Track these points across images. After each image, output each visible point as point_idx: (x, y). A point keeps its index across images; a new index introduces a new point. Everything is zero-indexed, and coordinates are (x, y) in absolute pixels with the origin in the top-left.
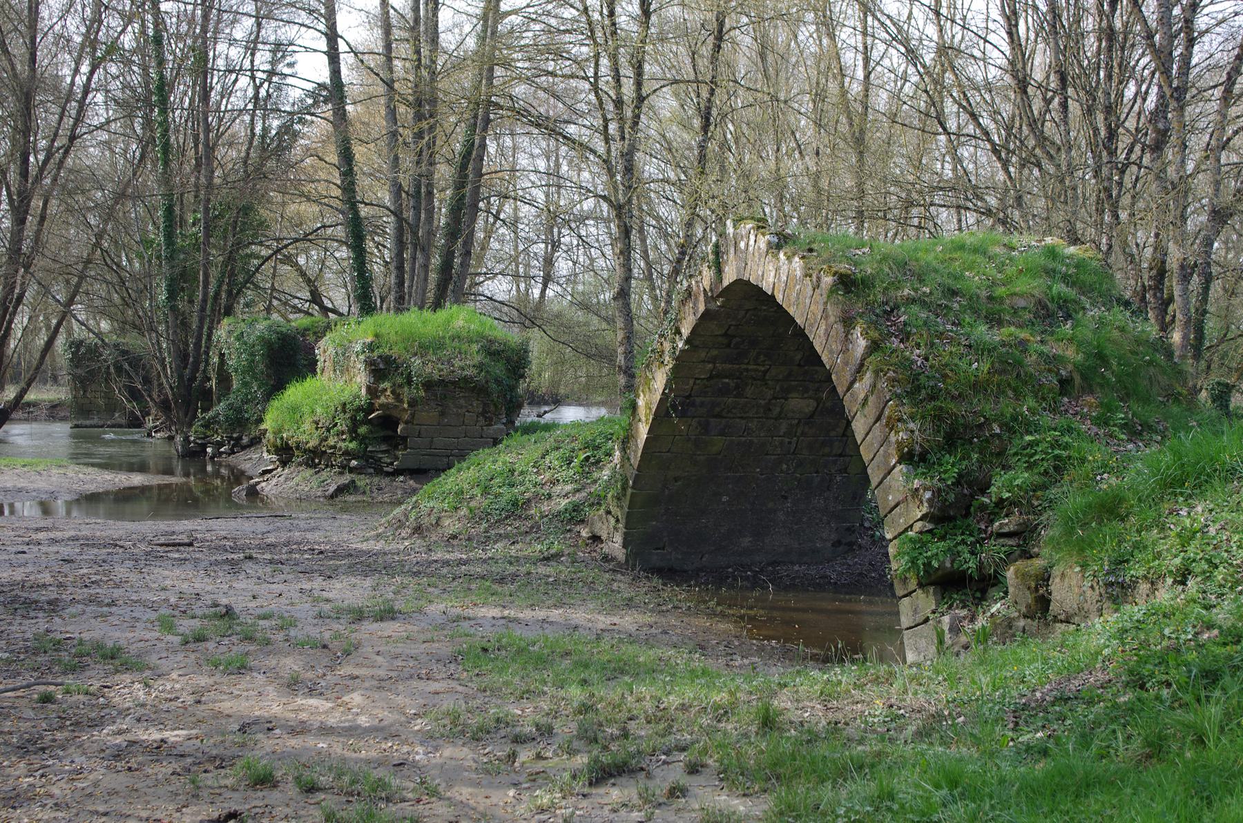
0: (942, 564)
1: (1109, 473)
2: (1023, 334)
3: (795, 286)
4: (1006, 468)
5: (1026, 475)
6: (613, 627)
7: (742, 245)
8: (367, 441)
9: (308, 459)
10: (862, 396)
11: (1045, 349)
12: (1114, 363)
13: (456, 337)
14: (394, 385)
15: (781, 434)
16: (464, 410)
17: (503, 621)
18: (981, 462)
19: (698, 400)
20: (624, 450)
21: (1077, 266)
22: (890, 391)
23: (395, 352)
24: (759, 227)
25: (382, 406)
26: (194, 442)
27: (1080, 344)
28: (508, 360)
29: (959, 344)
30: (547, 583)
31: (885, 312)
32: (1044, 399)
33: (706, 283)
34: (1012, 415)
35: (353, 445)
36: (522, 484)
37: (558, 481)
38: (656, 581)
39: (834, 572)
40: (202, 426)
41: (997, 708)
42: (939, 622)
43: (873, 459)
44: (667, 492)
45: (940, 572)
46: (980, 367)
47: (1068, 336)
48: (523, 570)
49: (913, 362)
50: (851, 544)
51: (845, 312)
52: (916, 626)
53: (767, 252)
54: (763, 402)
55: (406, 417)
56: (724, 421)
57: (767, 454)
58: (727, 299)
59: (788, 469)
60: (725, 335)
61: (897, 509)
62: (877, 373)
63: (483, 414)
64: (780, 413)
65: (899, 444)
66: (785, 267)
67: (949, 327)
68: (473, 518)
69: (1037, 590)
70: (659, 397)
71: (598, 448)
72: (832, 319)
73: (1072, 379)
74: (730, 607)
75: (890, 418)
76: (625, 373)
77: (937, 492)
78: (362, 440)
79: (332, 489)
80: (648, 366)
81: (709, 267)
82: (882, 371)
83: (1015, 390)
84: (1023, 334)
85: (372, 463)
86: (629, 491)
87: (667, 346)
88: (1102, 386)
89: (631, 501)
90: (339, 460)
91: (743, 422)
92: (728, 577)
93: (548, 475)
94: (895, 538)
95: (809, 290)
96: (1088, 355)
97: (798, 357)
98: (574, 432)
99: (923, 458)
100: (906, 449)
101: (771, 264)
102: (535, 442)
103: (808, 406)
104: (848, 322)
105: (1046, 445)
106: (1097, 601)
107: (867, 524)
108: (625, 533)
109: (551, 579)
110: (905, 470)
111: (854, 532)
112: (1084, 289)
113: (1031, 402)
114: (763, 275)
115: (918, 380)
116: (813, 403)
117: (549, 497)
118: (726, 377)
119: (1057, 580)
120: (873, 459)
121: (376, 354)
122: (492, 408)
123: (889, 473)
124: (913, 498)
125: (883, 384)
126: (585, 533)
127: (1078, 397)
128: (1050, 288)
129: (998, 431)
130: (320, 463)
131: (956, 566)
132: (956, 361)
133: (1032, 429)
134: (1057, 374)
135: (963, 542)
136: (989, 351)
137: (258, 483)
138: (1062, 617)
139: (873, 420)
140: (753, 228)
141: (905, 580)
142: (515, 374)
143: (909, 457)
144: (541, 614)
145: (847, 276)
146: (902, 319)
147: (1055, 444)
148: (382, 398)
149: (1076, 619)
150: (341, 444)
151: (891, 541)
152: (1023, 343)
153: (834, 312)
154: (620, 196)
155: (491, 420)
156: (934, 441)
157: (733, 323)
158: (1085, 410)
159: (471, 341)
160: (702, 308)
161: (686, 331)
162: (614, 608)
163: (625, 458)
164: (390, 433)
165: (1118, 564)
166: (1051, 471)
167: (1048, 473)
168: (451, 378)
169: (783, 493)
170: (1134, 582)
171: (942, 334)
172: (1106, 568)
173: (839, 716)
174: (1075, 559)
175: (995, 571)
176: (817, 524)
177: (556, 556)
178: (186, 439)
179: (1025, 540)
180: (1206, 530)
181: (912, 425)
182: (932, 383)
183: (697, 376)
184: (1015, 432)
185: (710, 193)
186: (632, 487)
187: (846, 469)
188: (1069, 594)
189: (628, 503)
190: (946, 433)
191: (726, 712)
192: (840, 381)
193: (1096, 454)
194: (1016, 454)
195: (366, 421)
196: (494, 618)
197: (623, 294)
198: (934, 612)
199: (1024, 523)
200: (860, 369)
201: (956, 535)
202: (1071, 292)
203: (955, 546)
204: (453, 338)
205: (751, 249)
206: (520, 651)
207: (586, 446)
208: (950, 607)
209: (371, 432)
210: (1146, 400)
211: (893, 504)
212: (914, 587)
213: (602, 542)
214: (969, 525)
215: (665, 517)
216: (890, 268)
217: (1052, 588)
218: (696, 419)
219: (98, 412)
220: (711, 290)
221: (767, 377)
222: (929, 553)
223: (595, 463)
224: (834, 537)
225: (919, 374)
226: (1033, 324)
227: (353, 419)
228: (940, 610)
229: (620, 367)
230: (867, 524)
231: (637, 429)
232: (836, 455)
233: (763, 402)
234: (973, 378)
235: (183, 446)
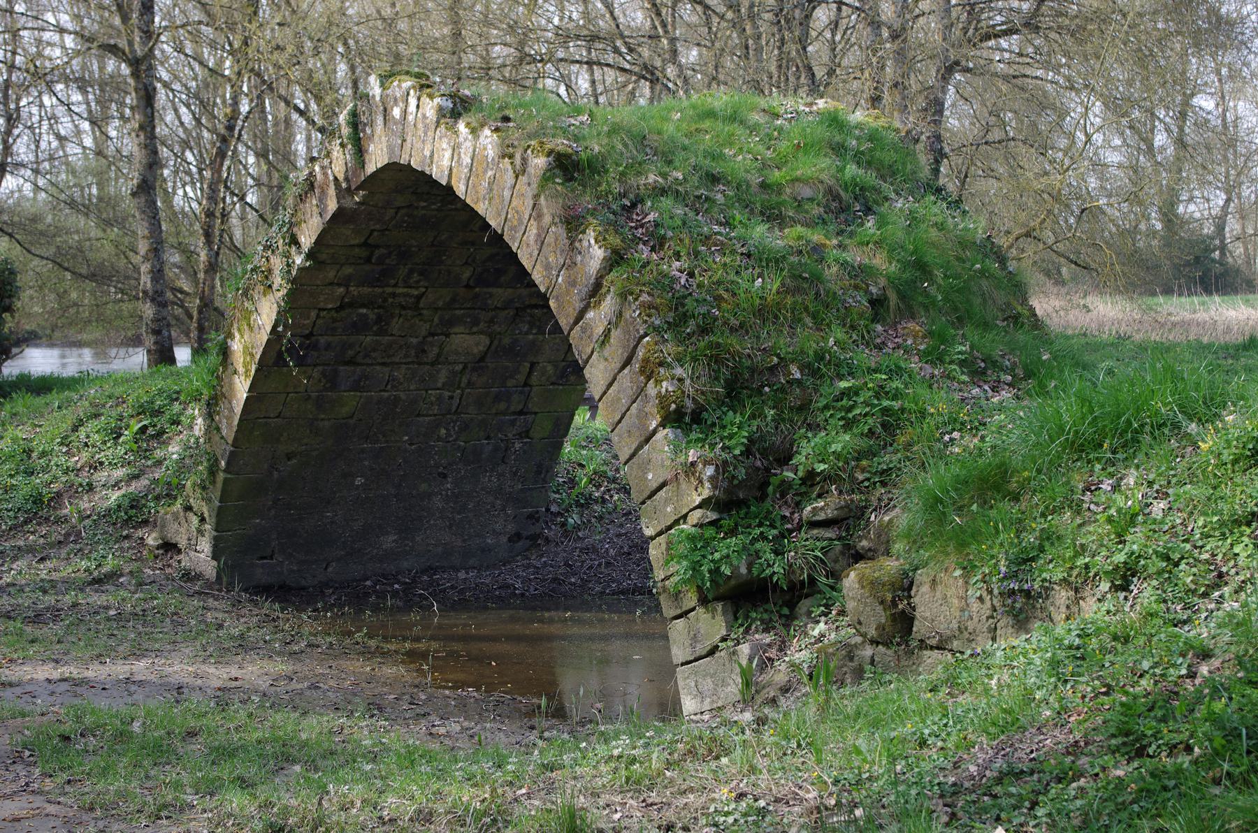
0: (735, 569)
1: (960, 430)
2: (816, 237)
3: (485, 172)
4: (814, 427)
5: (847, 437)
6: (234, 684)
7: (396, 112)
10: (600, 330)
11: (847, 256)
12: (939, 273)
15: (440, 385)
17: (64, 686)
18: (778, 420)
19: (322, 340)
20: (210, 416)
21: (871, 138)
22: (646, 322)
24: (422, 86)
27: (891, 251)
29: (733, 252)
30: (108, 619)
31: (624, 207)
32: (853, 328)
33: (338, 169)
34: (815, 352)
36: (45, 469)
37: (101, 463)
38: (269, 607)
39: (517, 577)
41: (913, 792)
42: (734, 653)
43: (619, 421)
44: (276, 474)
45: (733, 582)
46: (765, 285)
47: (875, 238)
48: (68, 599)
49: (674, 280)
50: (534, 538)
51: (566, 208)
52: (696, 660)
53: (438, 123)
54: (414, 341)
56: (358, 369)
57: (418, 415)
58: (371, 193)
59: (448, 435)
60: (365, 244)
61: (662, 493)
62: (623, 295)
64: (439, 355)
65: (663, 400)
66: (468, 144)
67: (716, 228)
69: (894, 603)
70: (265, 338)
71: (158, 413)
72: (547, 219)
73: (886, 298)
74: (386, 639)
75: (646, 361)
76: (153, 300)
80: (245, 293)
81: (342, 145)
82: (632, 294)
83: (814, 317)
84: (816, 237)
86: (221, 476)
87: (277, 263)
88: (927, 309)
89: (224, 491)
91: (386, 369)
92: (367, 595)
93: (86, 455)
94: (659, 534)
95: (509, 177)
96: (905, 265)
97: (467, 274)
98: (119, 390)
99: (697, 418)
100: (673, 406)
101: (445, 140)
102: (59, 407)
103: (477, 344)
104: (573, 223)
105: (871, 393)
106: (988, 618)
107: (554, 508)
108: (215, 538)
109: (112, 612)
110: (671, 436)
111: (538, 520)
112: (883, 172)
113: (839, 333)
114: (432, 156)
115: (683, 305)
116: (485, 340)
117: (90, 488)
118: (363, 306)
119: (925, 588)
120: (619, 421)
123: (647, 440)
124: (687, 476)
125: (633, 313)
126: (152, 540)
127: (895, 323)
128: (841, 170)
129: (798, 376)
131: (755, 572)
132: (732, 277)
133: (844, 371)
134: (867, 291)
135: (763, 537)
136: (777, 261)
138: (934, 642)
139: (619, 365)
140: (414, 87)
141: (677, 596)
143: (675, 418)
144: (120, 669)
145: (568, 156)
146: (651, 217)
147: (880, 392)
149: (956, 644)
151: (652, 538)
152: (818, 249)
153: (549, 208)
154: (136, 46)
156: (712, 392)
157: (378, 227)
160: (332, 206)
161: (307, 239)
162: (222, 655)
163: (212, 428)
165: (1019, 564)
166: (879, 430)
167: (873, 433)
169: (441, 470)
170: (1047, 590)
171: (708, 238)
172: (1003, 569)
173: (670, 815)
174: (953, 558)
175: (809, 575)
176: (488, 511)
177: (113, 576)
179: (848, 530)
180: (1147, 511)
181: (679, 371)
182: (703, 310)
183: (322, 305)
184: (822, 376)
185: (274, 43)
186: (225, 471)
187: (528, 432)
188: (943, 608)
189: (218, 494)
190: (726, 380)
191: (495, 821)
192: (563, 309)
193: (939, 403)
194: (826, 407)
196: (49, 681)
197: (147, 187)
198: (724, 639)
199: (847, 506)
200: (596, 291)
201: (749, 526)
202: (870, 177)
203: (752, 543)
205: (411, 118)
206: (122, 736)
207: (141, 411)
208: (747, 631)
210: (986, 326)
211: (655, 485)
212: (692, 604)
213: (179, 552)
214: (769, 512)
215: (273, 512)
216: (626, 145)
217: (916, 600)
218: (320, 368)
220: (347, 179)
221: (421, 305)
222: (717, 556)
223: (152, 436)
224: (511, 528)
225: (685, 297)
226: (824, 222)
228: (733, 636)
229: (145, 292)
230: (554, 508)
231: (231, 384)
232: (514, 413)
233: (414, 341)
234: (758, 301)
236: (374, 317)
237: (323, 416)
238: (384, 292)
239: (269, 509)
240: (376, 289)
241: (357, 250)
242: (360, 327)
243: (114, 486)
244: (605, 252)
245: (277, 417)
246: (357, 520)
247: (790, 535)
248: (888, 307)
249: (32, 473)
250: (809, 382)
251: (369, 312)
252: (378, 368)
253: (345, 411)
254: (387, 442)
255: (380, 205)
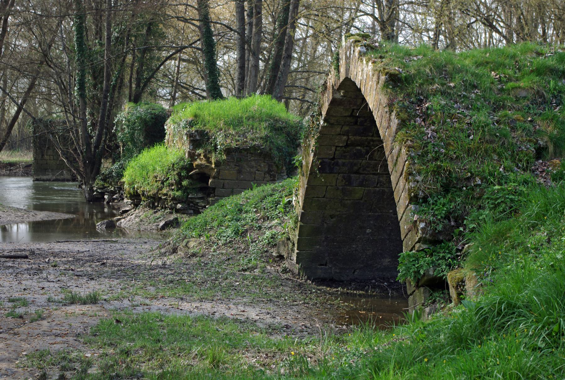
3: (369, 82)
8: (189, 191)
9: (150, 203)
13: (251, 118)
14: (206, 151)
16: (255, 169)
19: (340, 161)
23: (207, 129)
25: (198, 166)
26: (96, 191)
28: (288, 134)
35: (178, 193)
40: (102, 180)
44: (325, 225)
45: (426, 278)
53: (359, 58)
55: (213, 174)
56: (361, 176)
63: (269, 172)
68: (209, 242)
77: (429, 224)
78: (185, 190)
79: (162, 224)
85: (192, 206)
86: (299, 224)
90: (170, 204)
91: (376, 177)
100: (413, 194)
118: (358, 145)
121: (194, 129)
122: (275, 168)
129: (480, 182)
130: (158, 206)
135: (444, 258)
137: (119, 219)
142: (293, 144)
148: (198, 160)
150: (171, 193)
155: (274, 176)
158: (550, 169)
159: (261, 120)
164: (205, 185)
168: (244, 146)
178: (91, 190)
183: (337, 144)
195: (187, 177)
204: (248, 118)
209: (191, 184)
215: (325, 243)
218: (342, 175)
219: (52, 170)
225: (428, 143)
227: (179, 174)
235: (89, 194)
236: (365, 151)
237: (346, 198)
238: (367, 139)
239: (323, 242)
240: (363, 138)
241: (348, 119)
242: (359, 155)
243: (269, 228)
244: (398, 121)
245: (324, 197)
246: (369, 250)
247: (457, 258)
248: (548, 151)
249: (239, 220)
250: (484, 185)
251: (362, 148)
252: (371, 176)
253: (357, 196)
254: (381, 212)
255: (353, 97)
